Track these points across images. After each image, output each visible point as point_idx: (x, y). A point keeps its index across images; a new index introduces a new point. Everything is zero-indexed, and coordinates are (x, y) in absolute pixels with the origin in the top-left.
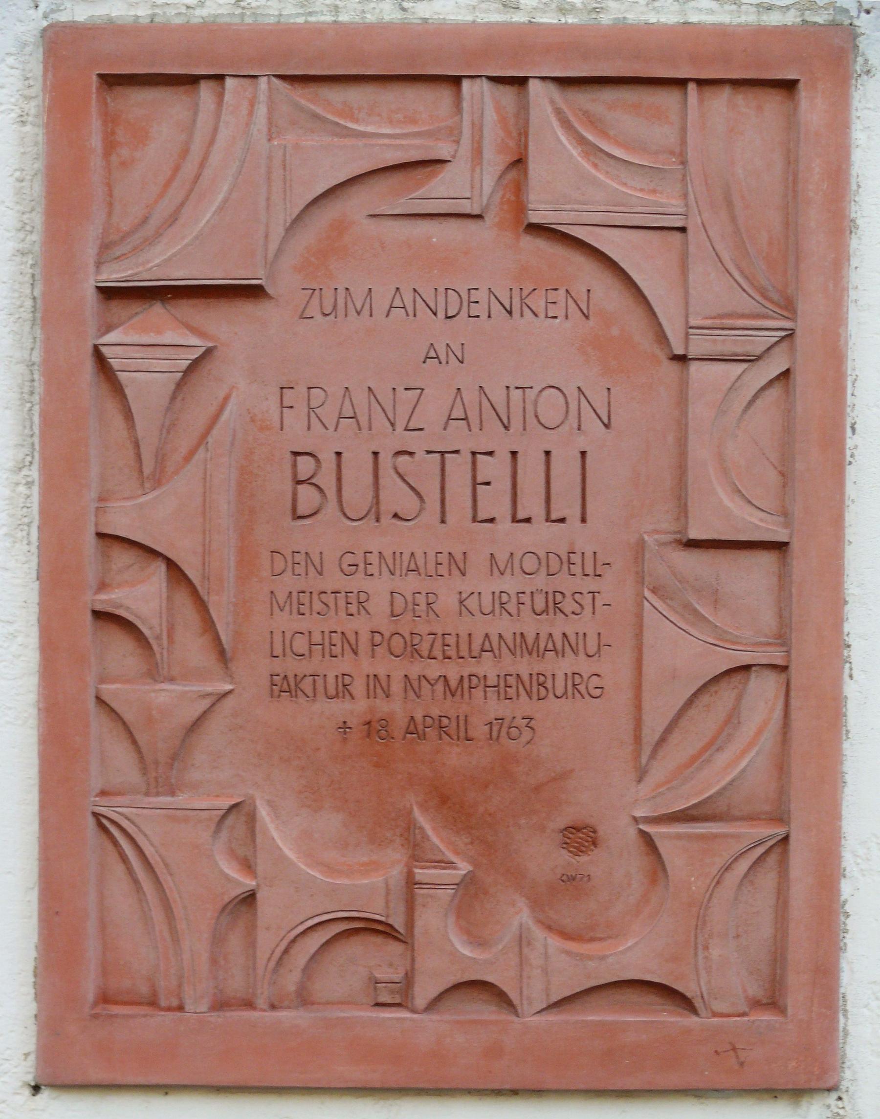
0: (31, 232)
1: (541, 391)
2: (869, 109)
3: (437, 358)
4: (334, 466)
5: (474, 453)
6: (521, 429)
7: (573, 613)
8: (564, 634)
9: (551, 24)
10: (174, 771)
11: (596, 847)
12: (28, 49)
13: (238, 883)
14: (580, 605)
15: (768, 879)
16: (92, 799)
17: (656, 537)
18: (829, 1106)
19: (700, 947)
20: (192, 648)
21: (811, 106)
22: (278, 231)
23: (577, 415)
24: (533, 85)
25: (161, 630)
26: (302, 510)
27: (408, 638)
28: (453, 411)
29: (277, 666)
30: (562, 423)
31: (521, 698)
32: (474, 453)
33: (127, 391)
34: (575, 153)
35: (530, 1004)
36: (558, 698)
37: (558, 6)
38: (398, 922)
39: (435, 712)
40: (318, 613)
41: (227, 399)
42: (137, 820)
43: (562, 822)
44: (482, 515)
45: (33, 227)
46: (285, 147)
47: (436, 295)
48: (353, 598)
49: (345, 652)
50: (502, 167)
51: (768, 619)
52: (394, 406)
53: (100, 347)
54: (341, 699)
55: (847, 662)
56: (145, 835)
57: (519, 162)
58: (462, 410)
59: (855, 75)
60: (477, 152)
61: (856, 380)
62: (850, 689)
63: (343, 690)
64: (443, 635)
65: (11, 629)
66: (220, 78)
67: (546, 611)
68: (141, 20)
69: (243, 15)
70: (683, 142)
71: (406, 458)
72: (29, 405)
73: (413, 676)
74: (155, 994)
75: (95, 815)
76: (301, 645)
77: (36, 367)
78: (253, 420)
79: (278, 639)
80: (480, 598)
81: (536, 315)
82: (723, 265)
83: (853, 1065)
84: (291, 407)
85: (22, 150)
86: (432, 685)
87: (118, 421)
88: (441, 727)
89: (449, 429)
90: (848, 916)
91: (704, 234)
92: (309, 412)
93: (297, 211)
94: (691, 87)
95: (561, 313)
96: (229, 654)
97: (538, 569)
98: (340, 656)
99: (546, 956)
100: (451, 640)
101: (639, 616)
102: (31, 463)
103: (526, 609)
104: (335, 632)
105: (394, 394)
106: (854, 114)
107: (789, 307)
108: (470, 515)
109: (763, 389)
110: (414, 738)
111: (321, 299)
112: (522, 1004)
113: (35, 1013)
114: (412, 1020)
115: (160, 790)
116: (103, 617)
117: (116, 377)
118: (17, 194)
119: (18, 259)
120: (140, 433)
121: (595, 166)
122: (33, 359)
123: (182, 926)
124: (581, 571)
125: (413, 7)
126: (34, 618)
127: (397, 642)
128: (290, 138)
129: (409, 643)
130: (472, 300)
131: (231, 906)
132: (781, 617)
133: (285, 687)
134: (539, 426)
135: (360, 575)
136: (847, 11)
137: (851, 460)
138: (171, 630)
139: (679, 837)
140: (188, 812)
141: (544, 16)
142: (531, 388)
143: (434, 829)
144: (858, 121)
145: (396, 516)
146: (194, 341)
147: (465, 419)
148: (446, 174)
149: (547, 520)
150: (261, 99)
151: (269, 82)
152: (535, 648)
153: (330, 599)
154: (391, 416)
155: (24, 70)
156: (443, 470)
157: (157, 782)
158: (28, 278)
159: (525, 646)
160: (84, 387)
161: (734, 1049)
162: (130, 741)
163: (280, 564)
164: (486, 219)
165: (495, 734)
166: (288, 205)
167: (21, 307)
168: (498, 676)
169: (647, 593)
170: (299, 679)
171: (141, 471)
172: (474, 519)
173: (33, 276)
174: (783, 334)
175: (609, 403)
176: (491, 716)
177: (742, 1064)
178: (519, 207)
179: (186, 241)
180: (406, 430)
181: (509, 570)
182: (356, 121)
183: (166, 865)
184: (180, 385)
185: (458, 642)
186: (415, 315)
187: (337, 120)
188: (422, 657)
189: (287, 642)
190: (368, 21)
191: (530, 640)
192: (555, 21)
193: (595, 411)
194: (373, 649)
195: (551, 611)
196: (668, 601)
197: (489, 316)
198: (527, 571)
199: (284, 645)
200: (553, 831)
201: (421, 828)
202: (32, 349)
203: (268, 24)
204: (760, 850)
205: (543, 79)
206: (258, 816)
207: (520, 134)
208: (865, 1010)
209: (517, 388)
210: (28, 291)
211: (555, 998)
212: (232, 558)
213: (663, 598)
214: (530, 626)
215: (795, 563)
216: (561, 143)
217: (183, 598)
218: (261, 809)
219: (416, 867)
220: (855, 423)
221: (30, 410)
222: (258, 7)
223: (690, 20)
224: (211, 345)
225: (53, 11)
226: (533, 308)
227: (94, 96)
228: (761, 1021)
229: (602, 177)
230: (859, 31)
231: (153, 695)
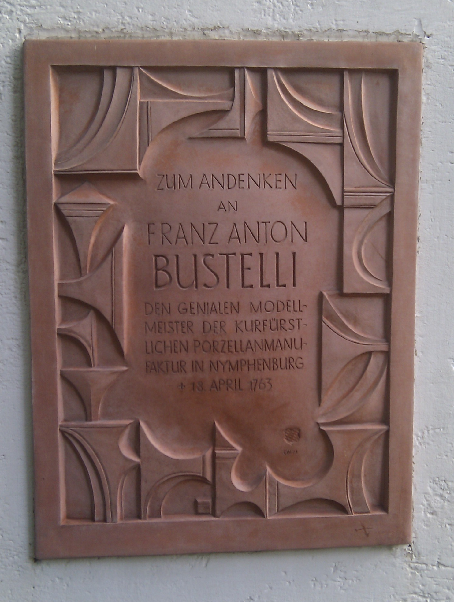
63: (181, 367)
69: (125, 37)
76: (160, 347)
79: (149, 345)
103: (267, 328)
127: (207, 346)
139: (339, 432)
159: (266, 345)
161: (364, 528)
180: (210, 243)
183: (97, 454)
191: (270, 342)
214: (270, 336)
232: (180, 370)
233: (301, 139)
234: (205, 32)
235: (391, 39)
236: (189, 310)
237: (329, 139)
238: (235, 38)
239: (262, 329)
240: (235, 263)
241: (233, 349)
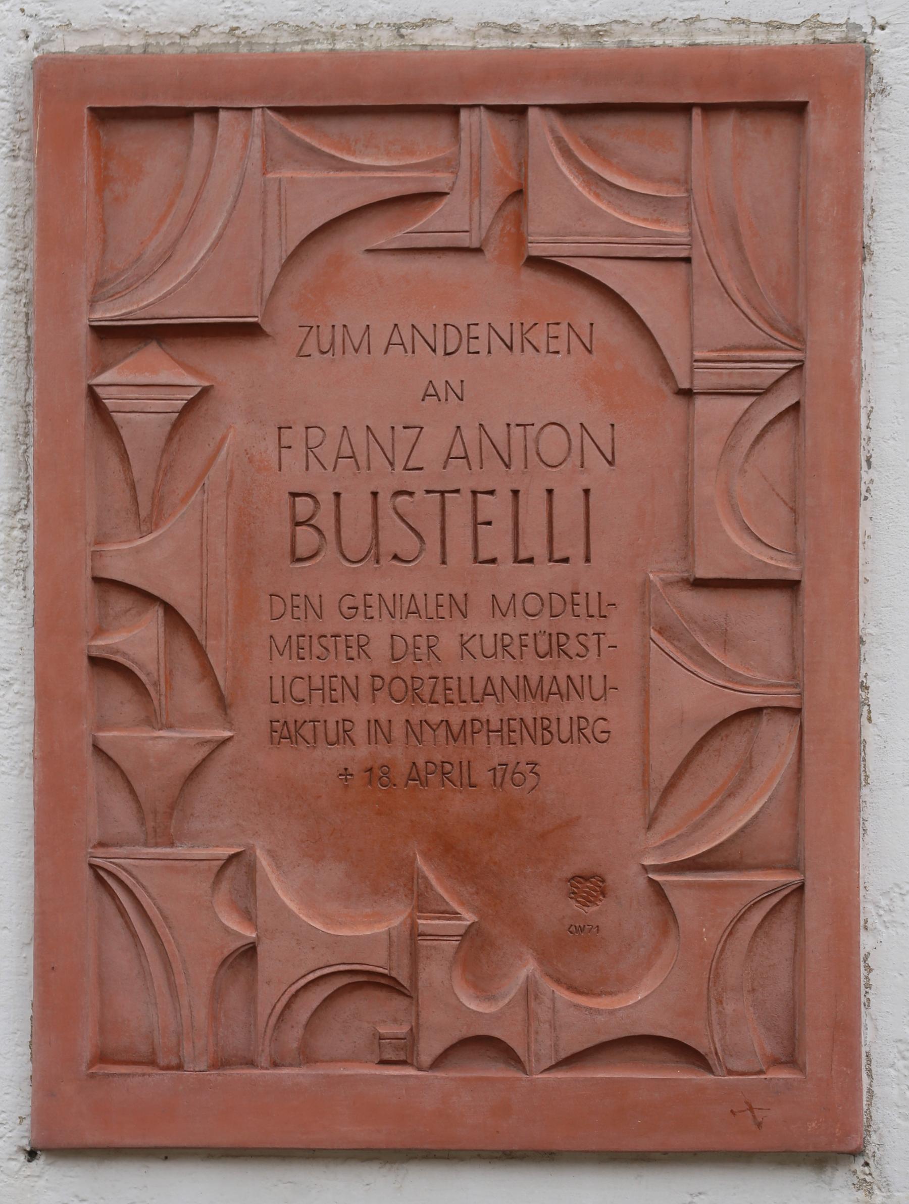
0: (25, 270)
1: (542, 428)
2: (884, 129)
3: (437, 395)
4: (333, 507)
5: (474, 493)
6: (523, 467)
7: (578, 655)
8: (569, 677)
9: (553, 48)
10: (173, 821)
11: (604, 897)
12: (19, 81)
13: (240, 936)
14: (584, 646)
15: (783, 932)
16: (90, 850)
17: (662, 575)
18: (855, 1172)
19: (713, 1001)
20: (192, 695)
21: (821, 131)
22: (273, 269)
23: (579, 453)
24: (532, 114)
25: (159, 676)
26: (301, 551)
27: (409, 682)
28: (454, 449)
29: (277, 712)
30: (565, 460)
31: (525, 743)
32: (474, 493)
33: (123, 432)
34: (576, 183)
35: (538, 1060)
36: (563, 742)
37: (560, 30)
38: (402, 976)
39: (438, 758)
40: (318, 657)
41: (223, 439)
42: (135, 872)
43: (568, 871)
44: (483, 556)
45: (27, 265)
46: (280, 181)
47: (435, 331)
48: (353, 641)
49: (346, 697)
50: (501, 199)
51: (780, 659)
52: (393, 445)
53: (95, 388)
54: (342, 745)
55: (865, 704)
56: (144, 887)
57: (519, 194)
58: (462, 449)
59: (869, 95)
60: (476, 183)
61: (871, 411)
62: (869, 733)
63: (345, 735)
64: (445, 678)
65: (7, 676)
66: (213, 111)
67: (549, 653)
68: (134, 51)
69: (237, 44)
70: (688, 169)
71: (406, 497)
72: (24, 447)
73: (415, 720)
74: (154, 1052)
75: (92, 866)
76: (300, 689)
77: (31, 408)
78: (251, 461)
79: (277, 683)
80: (481, 641)
81: (538, 351)
82: (729, 296)
83: (879, 1128)
84: (290, 447)
85: (14, 186)
86: (434, 731)
87: (114, 463)
88: (444, 774)
89: (449, 468)
90: (871, 970)
91: (710, 264)
92: (307, 453)
93: (292, 248)
94: (696, 114)
95: (563, 348)
96: (228, 701)
97: (541, 610)
98: (340, 702)
99: (554, 1010)
100: (453, 684)
101: (646, 657)
102: (26, 506)
103: (529, 651)
104: (336, 677)
105: (393, 433)
106: (867, 136)
107: (797, 336)
108: (471, 557)
109: (772, 423)
110: (417, 784)
111: (318, 336)
112: (529, 1061)
113: (30, 1074)
114: (417, 1077)
115: (159, 840)
116: (101, 664)
117: (111, 418)
118: (10, 231)
119: (12, 297)
120: (136, 475)
121: (597, 196)
122: (27, 400)
123: (180, 980)
124: (585, 611)
125: (411, 34)
126: (30, 666)
127: (398, 686)
128: (286, 174)
129: (410, 687)
130: (471, 336)
131: (231, 960)
132: (794, 658)
133: (285, 733)
134: (541, 464)
135: (360, 618)
136: (861, 27)
137: (867, 495)
138: (170, 674)
139: (689, 885)
140: (187, 863)
141: (546, 40)
142: (533, 425)
143: (437, 879)
144: (872, 142)
145: (395, 557)
146: (189, 380)
147: (466, 457)
148: (442, 205)
149: (550, 561)
150: (255, 132)
151: (263, 115)
152: (539, 692)
153: (329, 642)
154: (390, 455)
155: (15, 103)
156: (443, 509)
157: (155, 831)
158: (22, 317)
159: (526, 688)
160: (80, 426)
161: (751, 1109)
162: (127, 790)
163: (279, 608)
164: (486, 253)
165: (498, 780)
166: (284, 241)
167: (15, 346)
168: (502, 720)
169: (654, 634)
170: (299, 724)
171: (138, 514)
172: (475, 560)
173: (27, 314)
174: (792, 365)
175: (613, 439)
176: (495, 762)
177: (759, 1125)
178: (520, 239)
179: (181, 278)
180: (405, 469)
181: (511, 612)
182: (354, 153)
183: (165, 918)
184: (176, 426)
185: (459, 685)
186: (413, 352)
187: (333, 152)
188: (423, 701)
189: (287, 688)
190: (366, 49)
191: (534, 683)
192: (558, 46)
193: (598, 447)
194: (374, 694)
195: (555, 653)
196: (676, 643)
197: (489, 352)
198: (530, 612)
199: (283, 690)
200: (560, 880)
201: (425, 878)
202: (27, 390)
203: (263, 54)
204: (775, 900)
205: (543, 107)
206: (258, 866)
207: (520, 165)
208: (891, 1070)
209: (518, 425)
210: (23, 330)
211: (563, 1055)
212: (231, 602)
213: (670, 639)
214: (533, 669)
215: (806, 602)
216: (561, 173)
217: (182, 646)
218: (262, 859)
219: (419, 918)
220: (871, 456)
221: (25, 452)
222: (253, 36)
223: (697, 42)
224: (207, 384)
225: (43, 42)
226: (535, 343)
227: (86, 130)
228: (779, 1079)
229: (604, 207)
230: (873, 48)
231: (150, 742)
232: (342, 741)
233: (600, 249)
234: (403, 31)
235: (801, 37)
236: (361, 608)
237: (660, 251)
238: (464, 43)
239: (516, 653)
240: (458, 507)
241: (454, 697)
